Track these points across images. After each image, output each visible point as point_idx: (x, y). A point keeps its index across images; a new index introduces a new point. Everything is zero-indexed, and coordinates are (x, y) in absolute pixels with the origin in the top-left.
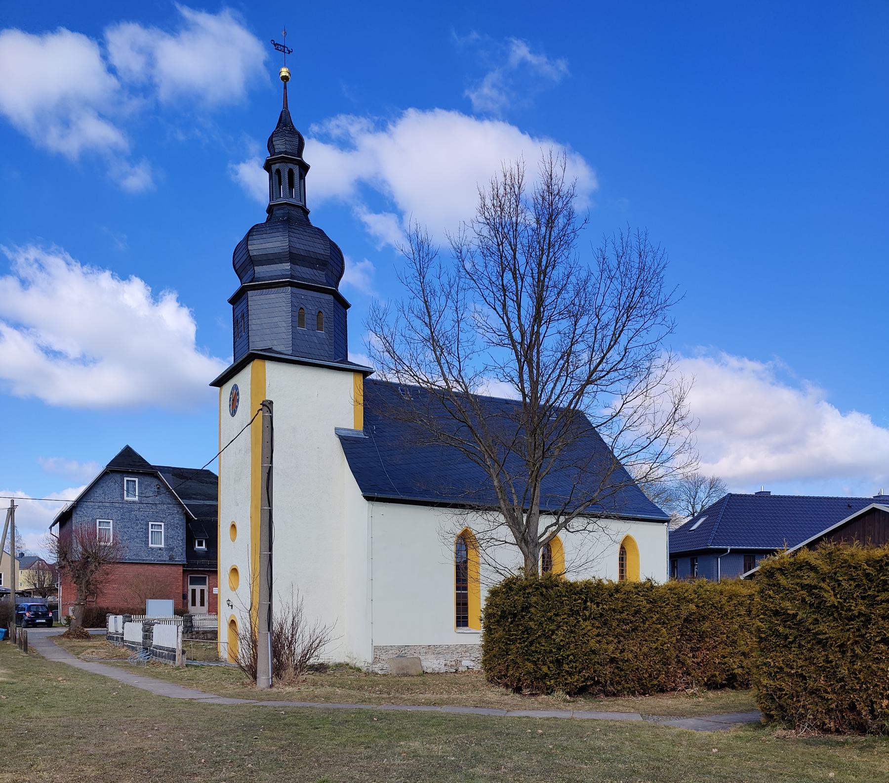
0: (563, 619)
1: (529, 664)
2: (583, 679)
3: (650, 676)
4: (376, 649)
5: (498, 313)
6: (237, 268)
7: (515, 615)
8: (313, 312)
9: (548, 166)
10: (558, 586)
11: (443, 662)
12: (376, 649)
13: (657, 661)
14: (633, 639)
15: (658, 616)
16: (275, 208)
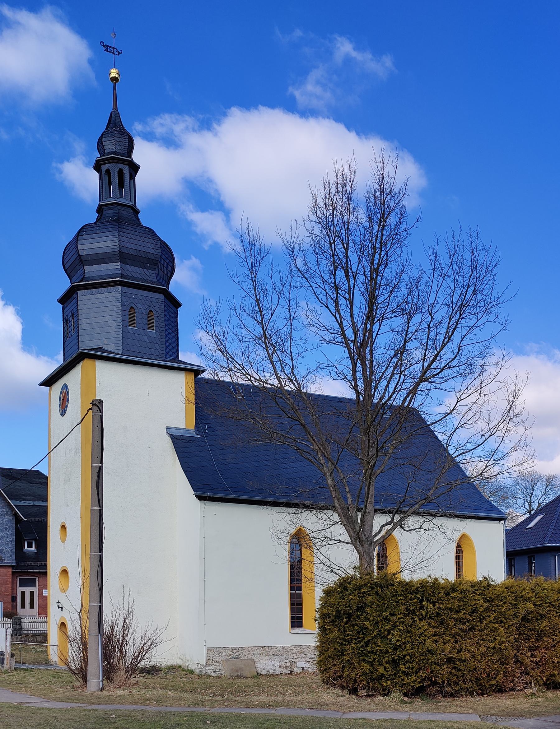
0: (399, 619)
2: (419, 680)
3: (488, 676)
4: (209, 650)
5: (330, 311)
7: (350, 616)
8: (144, 312)
10: (393, 585)
11: (277, 663)
12: (209, 650)
13: (495, 661)
14: (471, 639)
16: (105, 208)
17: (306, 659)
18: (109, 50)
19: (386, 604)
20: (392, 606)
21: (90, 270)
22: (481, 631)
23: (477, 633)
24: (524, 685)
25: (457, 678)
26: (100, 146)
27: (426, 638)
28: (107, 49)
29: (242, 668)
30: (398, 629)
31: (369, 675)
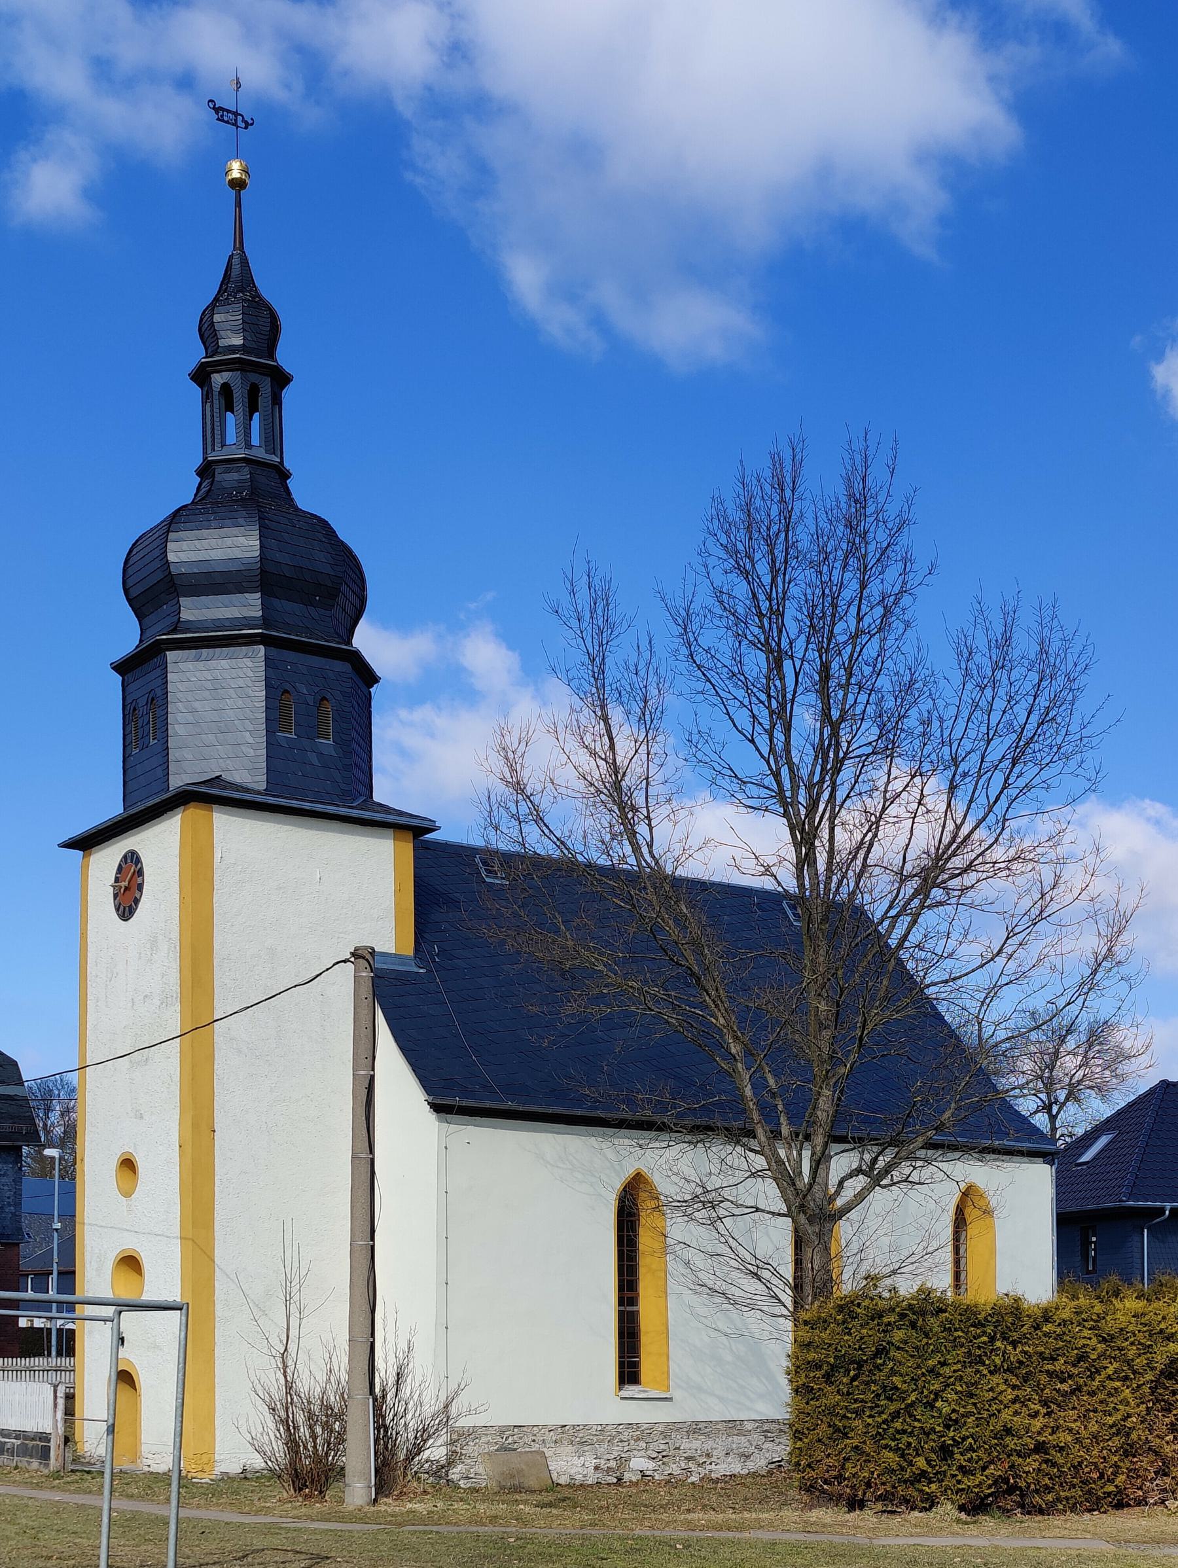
0: (955, 1371)
1: (891, 1455)
2: (990, 1482)
3: (1101, 1476)
5: (757, 749)
6: (134, 593)
7: (860, 1364)
9: (858, 460)
10: (945, 1311)
11: (591, 1462)
13: (1113, 1449)
14: (1074, 1408)
15: (1116, 1365)
16: (219, 469)
17: (649, 1452)
18: (225, 118)
19: (930, 1344)
20: (943, 1348)
21: (192, 610)
22: (1092, 1394)
23: (1085, 1398)
24: (1160, 1494)
25: (1049, 1479)
26: (208, 333)
27: (1002, 1407)
28: (222, 116)
29: (522, 1470)
30: (952, 1389)
31: (897, 1472)
